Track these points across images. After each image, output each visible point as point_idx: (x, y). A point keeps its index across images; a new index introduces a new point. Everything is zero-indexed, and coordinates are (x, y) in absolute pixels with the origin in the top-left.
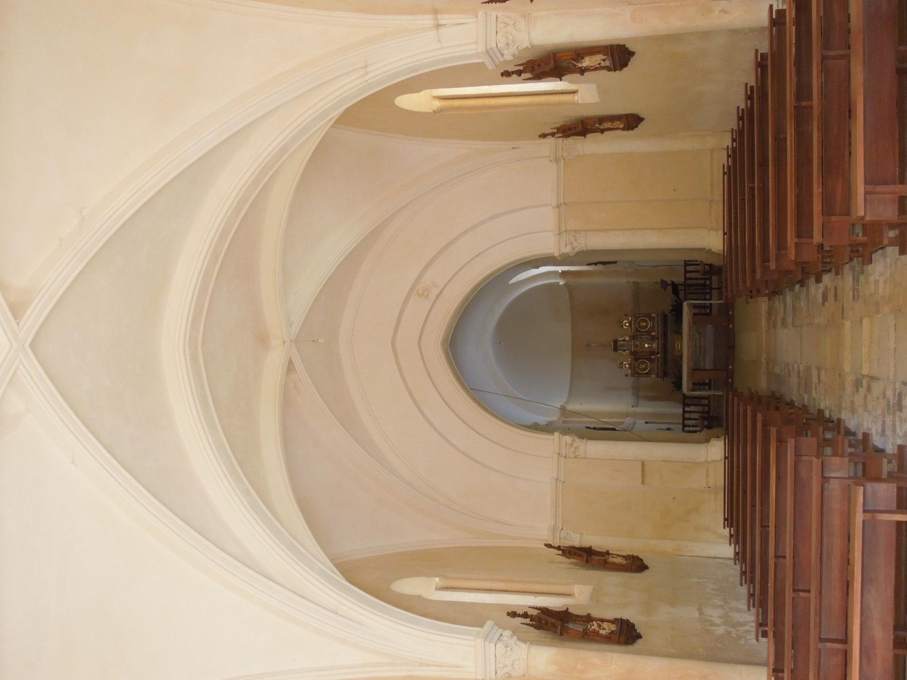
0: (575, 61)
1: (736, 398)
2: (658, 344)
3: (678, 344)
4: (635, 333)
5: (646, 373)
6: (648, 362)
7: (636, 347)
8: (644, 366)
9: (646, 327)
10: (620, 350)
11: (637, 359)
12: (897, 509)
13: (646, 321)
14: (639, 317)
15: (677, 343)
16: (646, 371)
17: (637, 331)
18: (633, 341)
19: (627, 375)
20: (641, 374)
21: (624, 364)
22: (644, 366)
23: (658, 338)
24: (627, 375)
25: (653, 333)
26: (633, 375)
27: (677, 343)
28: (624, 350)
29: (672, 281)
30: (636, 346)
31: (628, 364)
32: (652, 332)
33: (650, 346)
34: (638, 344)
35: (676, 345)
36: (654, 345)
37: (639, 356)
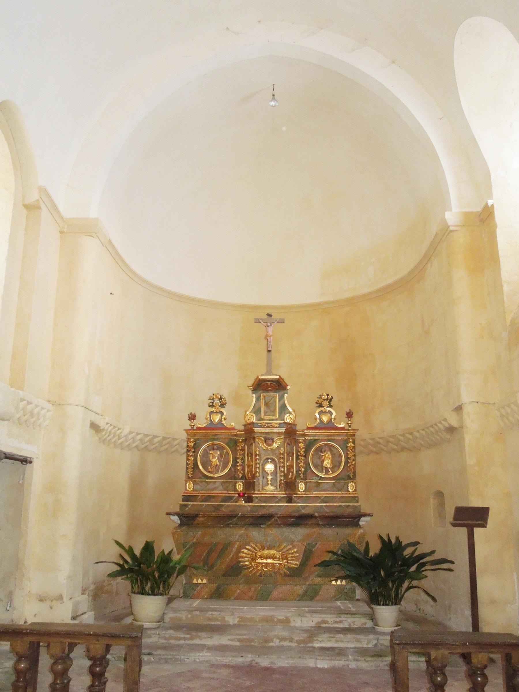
0: (246, 478)
1: (247, 547)
2: (272, 499)
3: (273, 557)
4: (302, 439)
5: (196, 465)
6: (226, 471)
7: (266, 440)
8: (215, 461)
9: (320, 467)
10: (258, 399)
11: (233, 443)
12: (492, 199)
13: (335, 466)
14: (345, 448)
15: (278, 555)
16: (201, 467)
17: (309, 445)
18: (283, 430)
19: (192, 417)
20: (195, 452)
21: (222, 410)
22: (215, 461)
23: (290, 500)
24: (192, 417)
25: (302, 486)
26: (191, 432)
27: (278, 555)
28: (257, 411)
29: (243, 425)
30: (269, 440)
31: (221, 420)
32: (306, 484)
33: (270, 477)
34: (275, 445)
35: (272, 552)
36: (270, 487)
37: (243, 450)
